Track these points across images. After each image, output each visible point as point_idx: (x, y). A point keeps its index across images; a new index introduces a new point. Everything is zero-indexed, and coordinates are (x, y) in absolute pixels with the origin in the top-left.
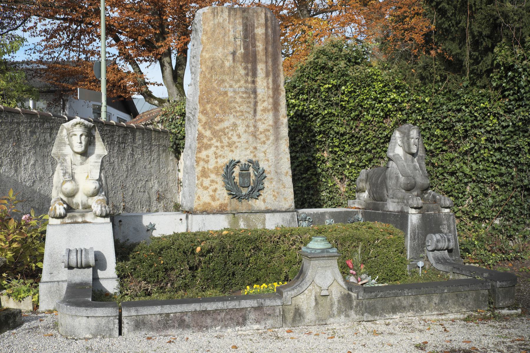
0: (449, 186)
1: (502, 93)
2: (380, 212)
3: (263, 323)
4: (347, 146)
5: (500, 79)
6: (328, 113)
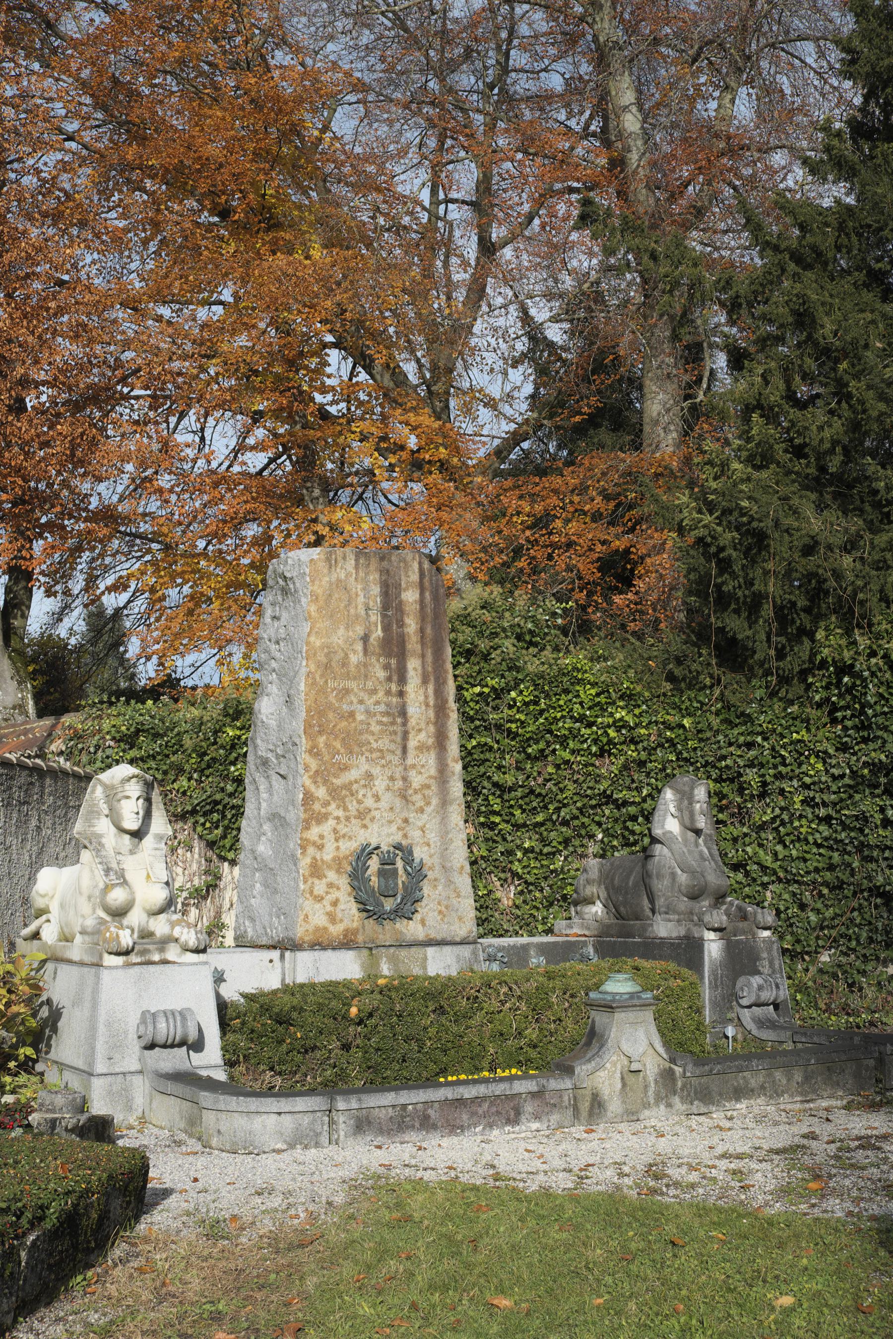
1: (830, 713)
2: (637, 940)
3: (545, 1119)
4: (518, 813)
5: (827, 688)
6: (479, 744)
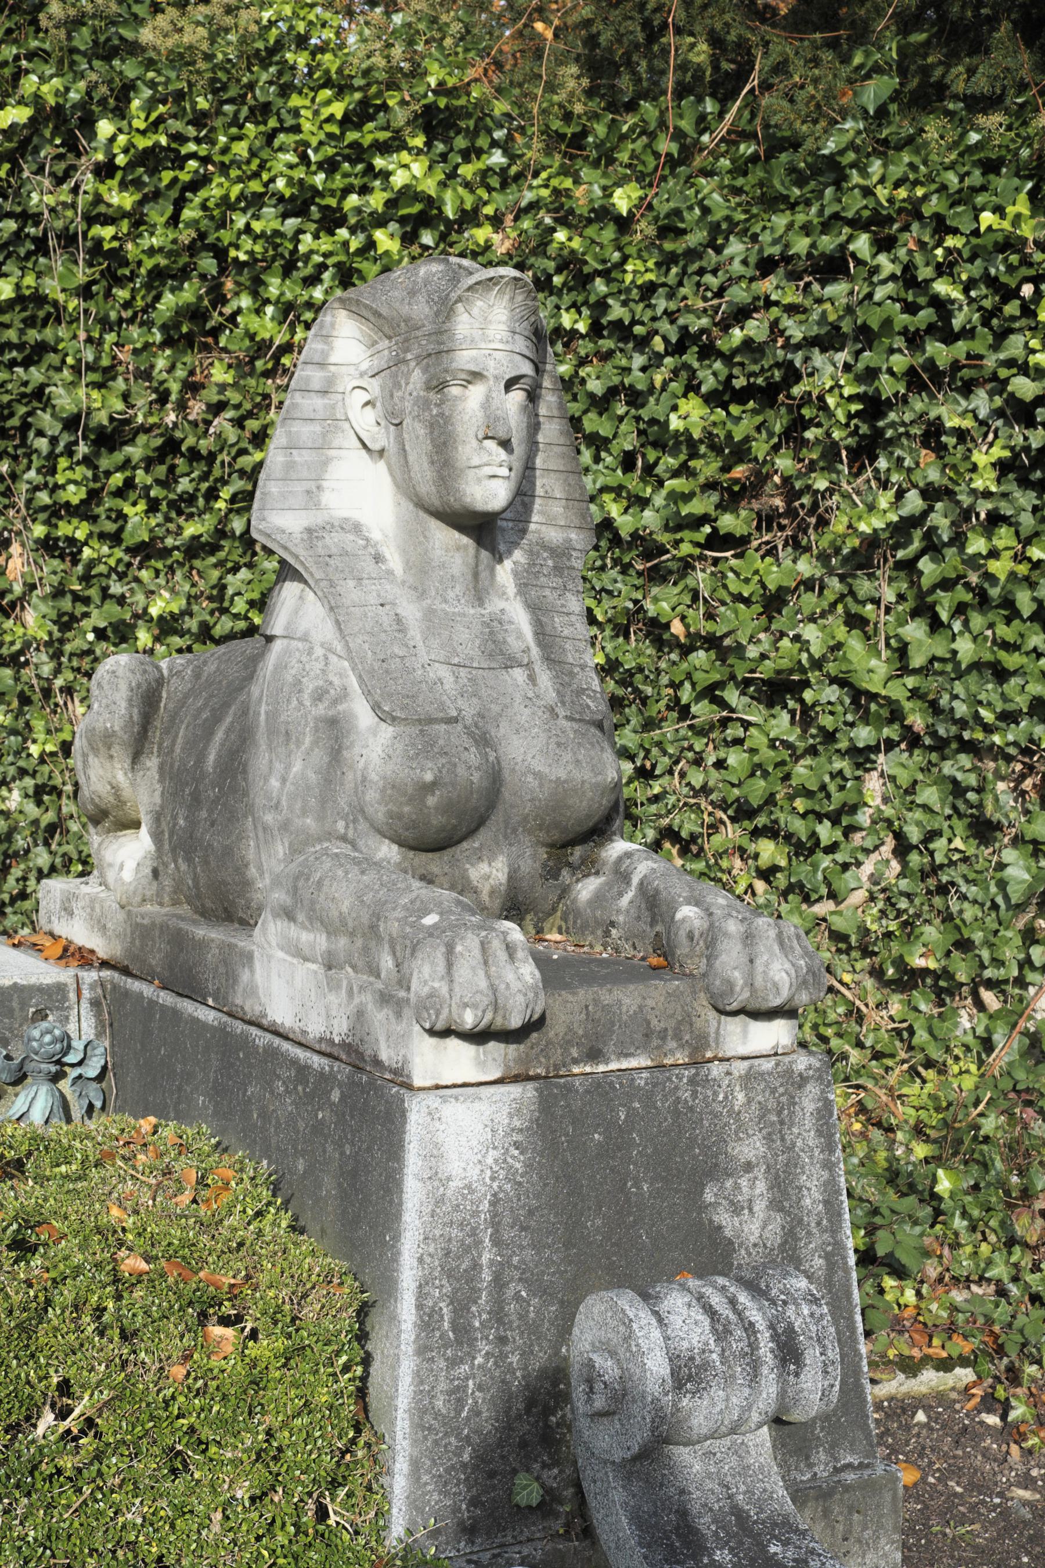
0: (757, 769)
2: (207, 1015)
4: (134, 511)
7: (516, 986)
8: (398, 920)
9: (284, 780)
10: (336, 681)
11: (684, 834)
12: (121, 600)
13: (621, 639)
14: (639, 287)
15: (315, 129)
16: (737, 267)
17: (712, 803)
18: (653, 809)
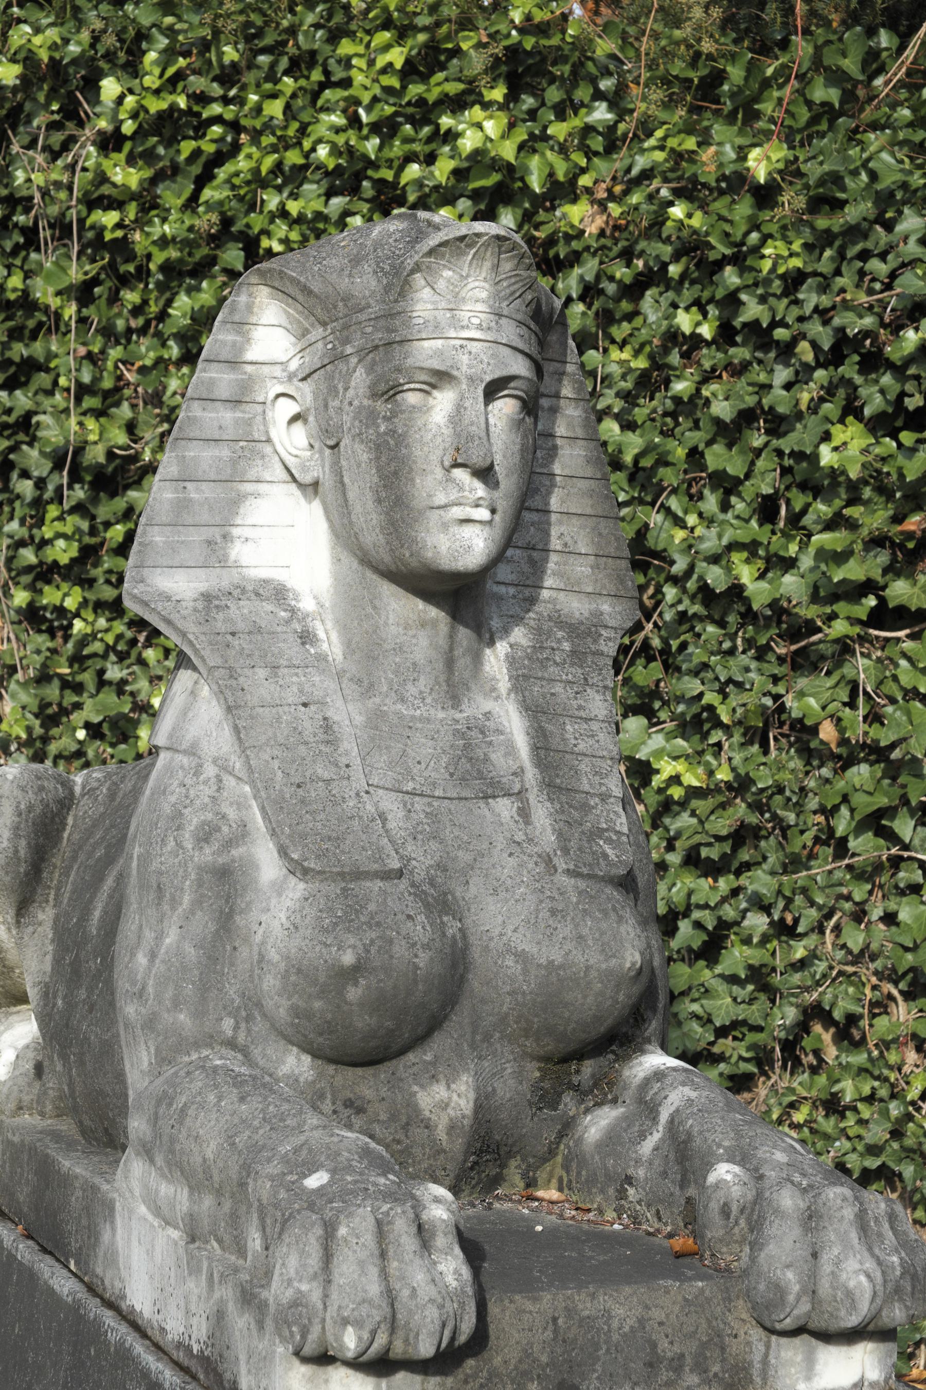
2: (64, 1285)
7: (426, 1291)
8: (272, 1178)
9: (153, 956)
10: (232, 813)
11: (837, 1015)
12: (120, 687)
13: (755, 748)
14: (783, 277)
15: (368, 82)
16: (912, 248)
17: (876, 973)
18: (796, 978)
